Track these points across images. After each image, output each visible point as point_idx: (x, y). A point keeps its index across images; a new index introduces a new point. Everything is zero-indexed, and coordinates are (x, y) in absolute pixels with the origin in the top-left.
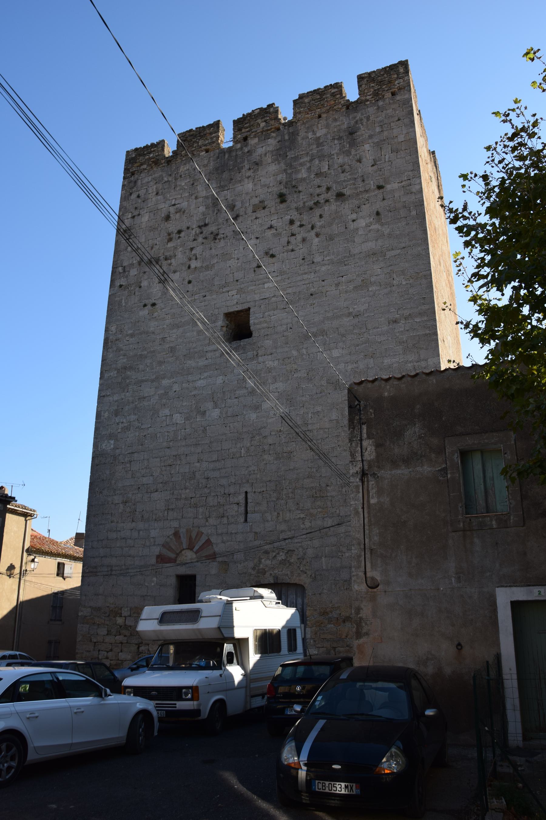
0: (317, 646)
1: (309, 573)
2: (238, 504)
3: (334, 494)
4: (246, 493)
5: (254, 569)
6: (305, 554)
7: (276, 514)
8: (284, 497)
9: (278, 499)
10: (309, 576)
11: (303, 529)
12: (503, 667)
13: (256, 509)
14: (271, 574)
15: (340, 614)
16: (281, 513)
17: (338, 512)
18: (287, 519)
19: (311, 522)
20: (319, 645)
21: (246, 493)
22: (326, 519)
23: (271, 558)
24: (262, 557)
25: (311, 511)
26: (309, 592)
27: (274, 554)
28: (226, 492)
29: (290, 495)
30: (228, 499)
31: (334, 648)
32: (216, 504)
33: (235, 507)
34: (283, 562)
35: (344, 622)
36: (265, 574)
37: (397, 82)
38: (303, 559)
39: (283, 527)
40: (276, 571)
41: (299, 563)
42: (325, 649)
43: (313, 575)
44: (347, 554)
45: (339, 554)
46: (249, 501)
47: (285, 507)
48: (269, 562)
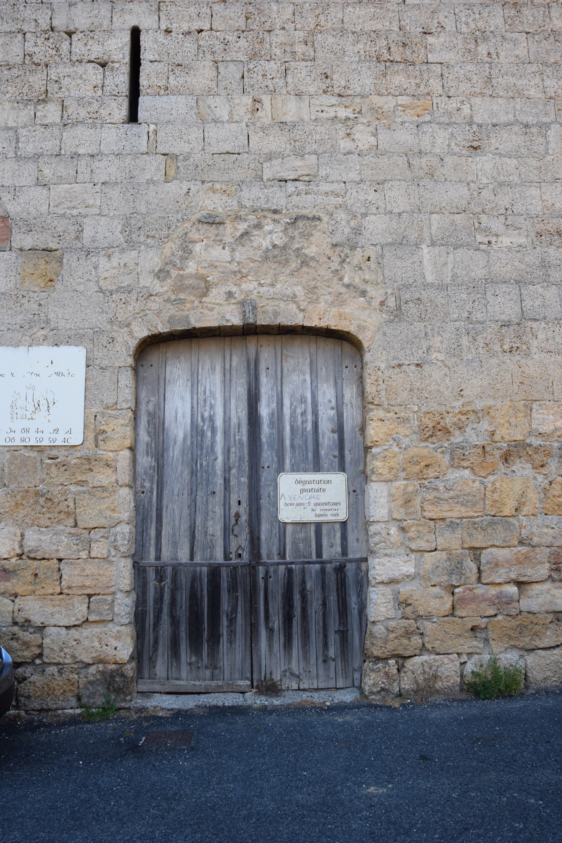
0: (413, 546)
1: (376, 294)
2: (103, 65)
3: (446, 57)
4: (136, 33)
5: (161, 274)
6: (357, 231)
7: (247, 100)
8: (278, 51)
9: (254, 56)
10: (376, 304)
11: (349, 153)
12: (246, 406)
13: (172, 82)
14: (230, 295)
15: (493, 434)
16: (266, 99)
17: (466, 110)
18: (288, 119)
19: (375, 135)
20: (423, 545)
21: (136, 33)
22: (425, 128)
23: (228, 239)
24: (194, 235)
25: (377, 101)
26: (376, 358)
27: (242, 227)
28: (55, 23)
29: (300, 49)
30: (65, 46)
31: (476, 552)
32: (19, 60)
33: (93, 74)
34: (276, 255)
35: (506, 458)
36: (205, 295)
37: (165, 288)
38: (353, 248)
39: (276, 142)
40: (249, 285)
41: (336, 259)
42: (444, 555)
43: (391, 302)
44: (506, 241)
45: (479, 238)
46: (146, 56)
47: (281, 83)
48: (219, 254)
